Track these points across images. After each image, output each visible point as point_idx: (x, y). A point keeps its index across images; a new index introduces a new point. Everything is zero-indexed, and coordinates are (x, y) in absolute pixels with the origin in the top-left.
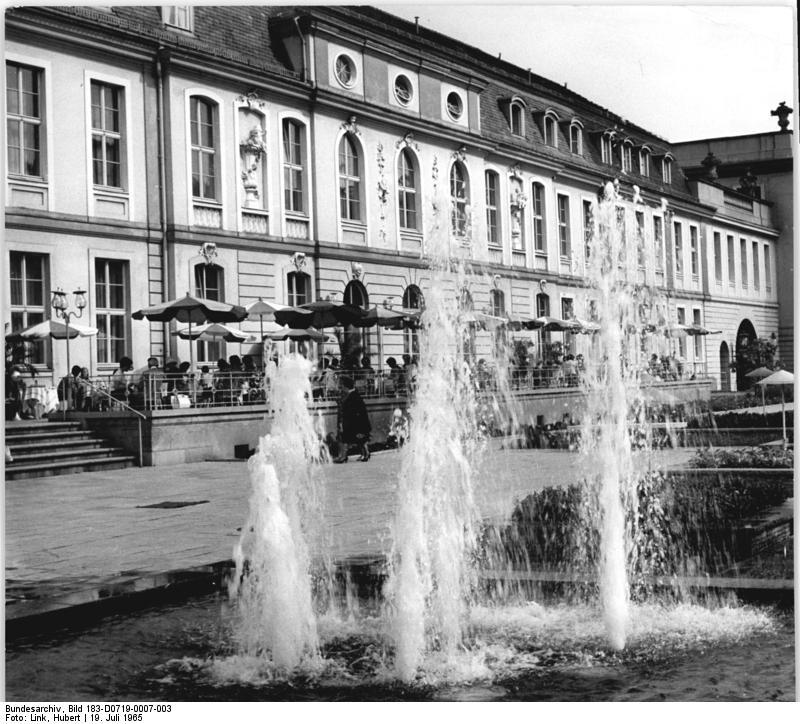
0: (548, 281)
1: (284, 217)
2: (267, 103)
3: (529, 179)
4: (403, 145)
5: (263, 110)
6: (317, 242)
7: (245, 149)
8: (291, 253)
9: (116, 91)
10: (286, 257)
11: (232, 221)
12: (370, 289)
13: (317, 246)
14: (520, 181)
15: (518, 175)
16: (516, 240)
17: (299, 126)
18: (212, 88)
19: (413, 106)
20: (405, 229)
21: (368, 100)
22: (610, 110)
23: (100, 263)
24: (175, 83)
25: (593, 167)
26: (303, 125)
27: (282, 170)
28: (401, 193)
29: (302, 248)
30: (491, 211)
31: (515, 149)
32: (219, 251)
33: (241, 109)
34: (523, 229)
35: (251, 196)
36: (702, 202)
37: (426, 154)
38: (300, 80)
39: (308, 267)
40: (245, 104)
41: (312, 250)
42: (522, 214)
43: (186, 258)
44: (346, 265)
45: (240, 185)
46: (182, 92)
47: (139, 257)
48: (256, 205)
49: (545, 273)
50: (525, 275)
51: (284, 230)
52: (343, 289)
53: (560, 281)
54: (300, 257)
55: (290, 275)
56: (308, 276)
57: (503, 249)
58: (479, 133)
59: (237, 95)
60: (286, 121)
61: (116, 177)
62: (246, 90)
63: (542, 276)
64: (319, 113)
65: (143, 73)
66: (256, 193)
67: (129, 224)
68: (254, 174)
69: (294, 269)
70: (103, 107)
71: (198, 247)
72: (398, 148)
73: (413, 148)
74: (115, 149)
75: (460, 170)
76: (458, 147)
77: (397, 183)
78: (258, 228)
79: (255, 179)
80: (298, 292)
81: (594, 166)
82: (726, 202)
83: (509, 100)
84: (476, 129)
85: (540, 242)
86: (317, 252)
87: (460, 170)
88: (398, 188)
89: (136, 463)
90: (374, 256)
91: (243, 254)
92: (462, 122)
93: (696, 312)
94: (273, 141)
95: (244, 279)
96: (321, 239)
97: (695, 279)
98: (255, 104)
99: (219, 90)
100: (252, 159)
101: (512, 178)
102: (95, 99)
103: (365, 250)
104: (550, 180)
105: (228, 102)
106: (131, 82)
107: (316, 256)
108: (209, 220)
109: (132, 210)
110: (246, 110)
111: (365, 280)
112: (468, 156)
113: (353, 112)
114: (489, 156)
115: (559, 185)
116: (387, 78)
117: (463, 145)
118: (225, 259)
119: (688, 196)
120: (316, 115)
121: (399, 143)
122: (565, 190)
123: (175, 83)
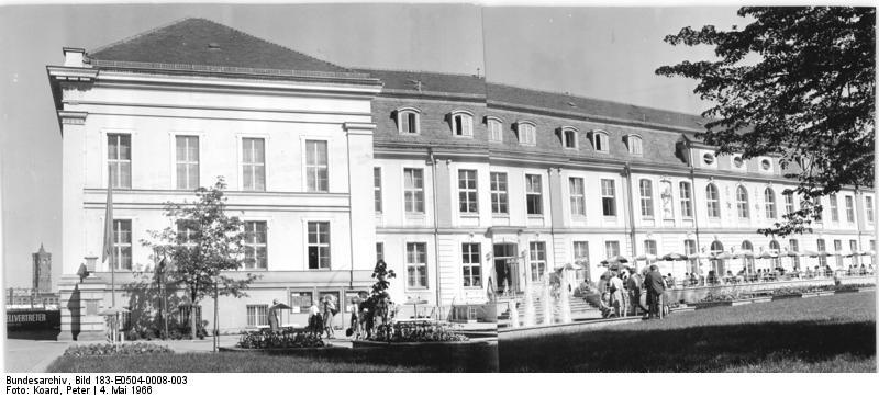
7: (663, 196)
13: (552, 233)
17: (687, 185)
20: (646, 216)
24: (633, 175)
28: (643, 200)
37: (750, 186)
43: (640, 239)
44: (712, 235)
46: (636, 178)
47: (624, 241)
48: (669, 216)
60: (642, 181)
61: (421, 208)
74: (420, 196)
78: (671, 224)
79: (669, 206)
83: (592, 133)
88: (737, 202)
91: (665, 235)
94: (676, 191)
96: (699, 226)
98: (667, 178)
100: (666, 199)
102: (603, 185)
105: (655, 179)
106: (616, 177)
107: (697, 233)
110: (663, 181)
111: (719, 239)
118: (721, 238)
123: (633, 175)
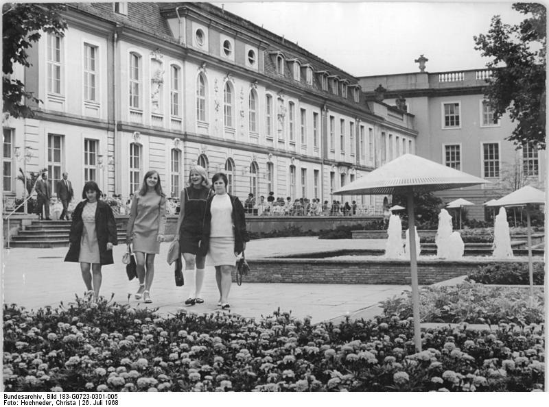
0: (296, 158)
1: (170, 118)
2: (164, 56)
3: (287, 99)
4: (227, 79)
5: (162, 60)
6: (186, 132)
8: (173, 138)
9: (93, 48)
10: (171, 140)
11: (147, 121)
12: (210, 159)
14: (282, 101)
15: (282, 98)
16: (280, 134)
18: (97, 37)
19: (231, 58)
21: (210, 54)
22: (286, 38)
23: (50, 136)
25: (319, 93)
26: (180, 68)
27: (83, 73)
29: (178, 136)
30: (201, 100)
31: (283, 83)
32: (141, 136)
33: (152, 59)
34: (283, 128)
35: (155, 107)
36: (375, 114)
38: (372, 114)
39: (181, 146)
40: (154, 57)
41: (183, 137)
42: (283, 119)
45: (151, 100)
46: (124, 48)
49: (271, 149)
50: (282, 154)
51: (83, 112)
52: (225, 162)
53: (302, 158)
54: (177, 140)
55: (172, 150)
56: (181, 151)
57: (143, 113)
58: (263, 74)
59: (151, 51)
62: (156, 49)
63: (293, 155)
64: (188, 61)
65: (107, 40)
66: (157, 105)
67: (100, 121)
68: (157, 95)
69: (174, 147)
70: (52, 48)
71: (131, 134)
72: (224, 81)
73: (232, 81)
75: (253, 93)
76: (253, 81)
77: (196, 93)
80: (91, 151)
81: (319, 92)
82: (388, 115)
84: (262, 70)
85: (253, 127)
86: (185, 138)
87: (253, 93)
89: (453, 229)
90: (211, 141)
92: (254, 67)
93: (316, 172)
95: (153, 152)
97: (316, 149)
98: (158, 57)
99: (141, 48)
100: (156, 86)
101: (279, 99)
103: (207, 137)
104: (297, 100)
105: (146, 54)
106: (101, 43)
108: (135, 119)
109: (66, 106)
110: (279, 99)
111: (207, 154)
112: (258, 86)
113: (204, 61)
114: (268, 87)
115: (302, 103)
116: (219, 42)
117: (256, 80)
119: (367, 110)
120: (186, 62)
121: (225, 78)
122: (304, 106)
